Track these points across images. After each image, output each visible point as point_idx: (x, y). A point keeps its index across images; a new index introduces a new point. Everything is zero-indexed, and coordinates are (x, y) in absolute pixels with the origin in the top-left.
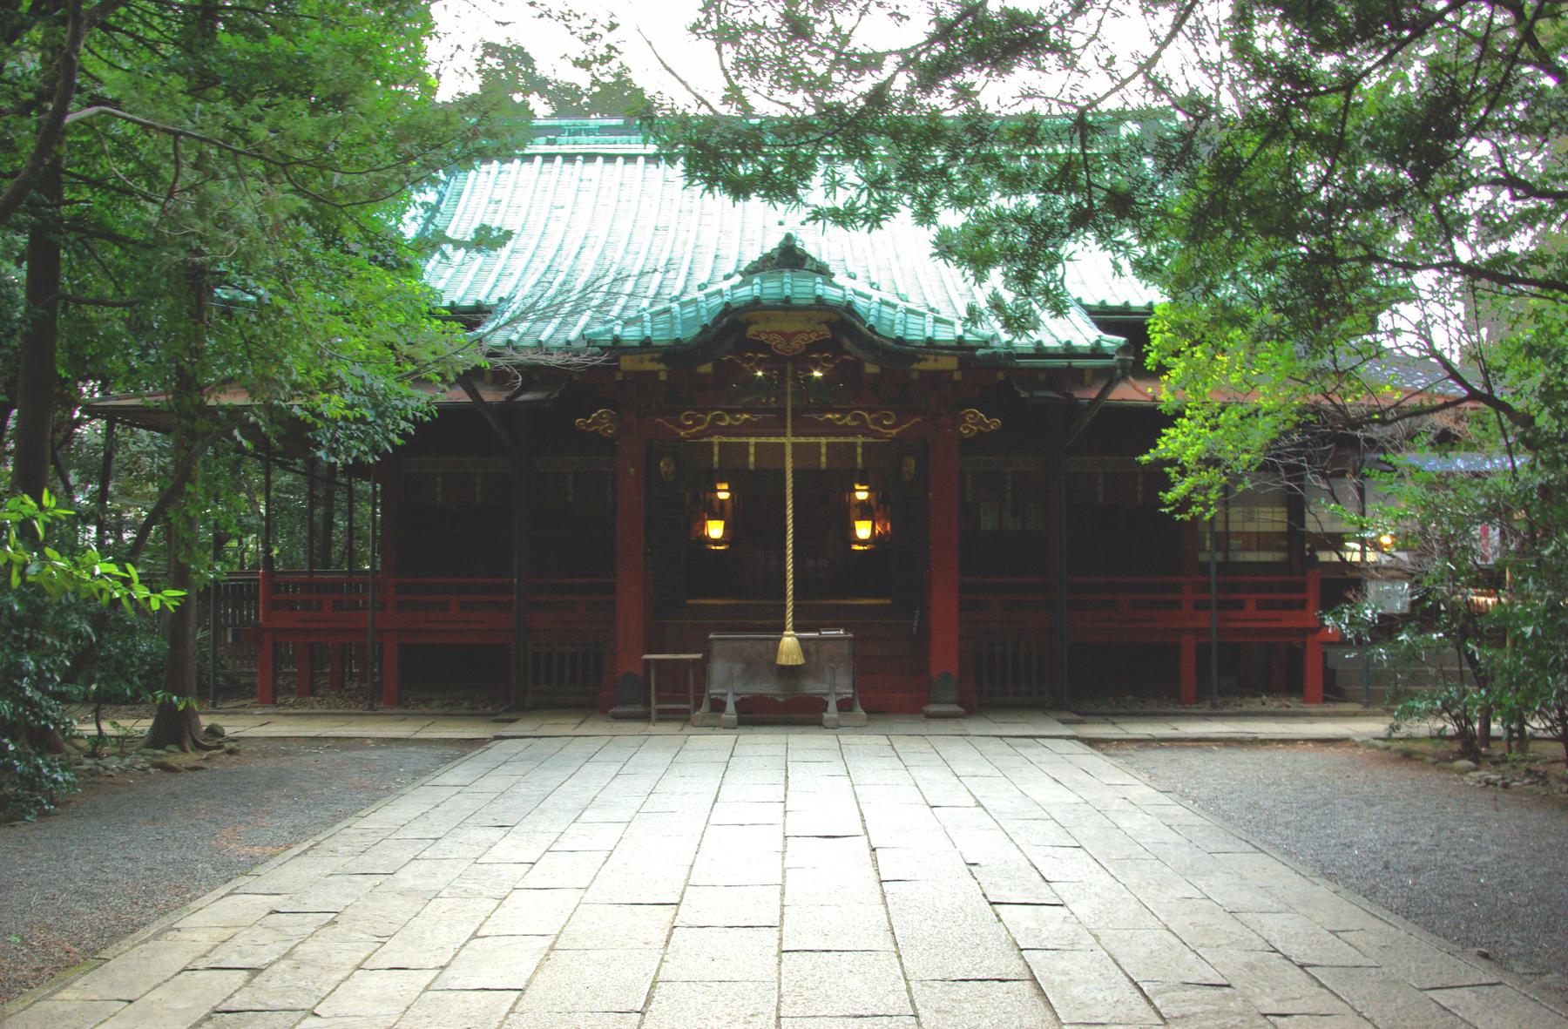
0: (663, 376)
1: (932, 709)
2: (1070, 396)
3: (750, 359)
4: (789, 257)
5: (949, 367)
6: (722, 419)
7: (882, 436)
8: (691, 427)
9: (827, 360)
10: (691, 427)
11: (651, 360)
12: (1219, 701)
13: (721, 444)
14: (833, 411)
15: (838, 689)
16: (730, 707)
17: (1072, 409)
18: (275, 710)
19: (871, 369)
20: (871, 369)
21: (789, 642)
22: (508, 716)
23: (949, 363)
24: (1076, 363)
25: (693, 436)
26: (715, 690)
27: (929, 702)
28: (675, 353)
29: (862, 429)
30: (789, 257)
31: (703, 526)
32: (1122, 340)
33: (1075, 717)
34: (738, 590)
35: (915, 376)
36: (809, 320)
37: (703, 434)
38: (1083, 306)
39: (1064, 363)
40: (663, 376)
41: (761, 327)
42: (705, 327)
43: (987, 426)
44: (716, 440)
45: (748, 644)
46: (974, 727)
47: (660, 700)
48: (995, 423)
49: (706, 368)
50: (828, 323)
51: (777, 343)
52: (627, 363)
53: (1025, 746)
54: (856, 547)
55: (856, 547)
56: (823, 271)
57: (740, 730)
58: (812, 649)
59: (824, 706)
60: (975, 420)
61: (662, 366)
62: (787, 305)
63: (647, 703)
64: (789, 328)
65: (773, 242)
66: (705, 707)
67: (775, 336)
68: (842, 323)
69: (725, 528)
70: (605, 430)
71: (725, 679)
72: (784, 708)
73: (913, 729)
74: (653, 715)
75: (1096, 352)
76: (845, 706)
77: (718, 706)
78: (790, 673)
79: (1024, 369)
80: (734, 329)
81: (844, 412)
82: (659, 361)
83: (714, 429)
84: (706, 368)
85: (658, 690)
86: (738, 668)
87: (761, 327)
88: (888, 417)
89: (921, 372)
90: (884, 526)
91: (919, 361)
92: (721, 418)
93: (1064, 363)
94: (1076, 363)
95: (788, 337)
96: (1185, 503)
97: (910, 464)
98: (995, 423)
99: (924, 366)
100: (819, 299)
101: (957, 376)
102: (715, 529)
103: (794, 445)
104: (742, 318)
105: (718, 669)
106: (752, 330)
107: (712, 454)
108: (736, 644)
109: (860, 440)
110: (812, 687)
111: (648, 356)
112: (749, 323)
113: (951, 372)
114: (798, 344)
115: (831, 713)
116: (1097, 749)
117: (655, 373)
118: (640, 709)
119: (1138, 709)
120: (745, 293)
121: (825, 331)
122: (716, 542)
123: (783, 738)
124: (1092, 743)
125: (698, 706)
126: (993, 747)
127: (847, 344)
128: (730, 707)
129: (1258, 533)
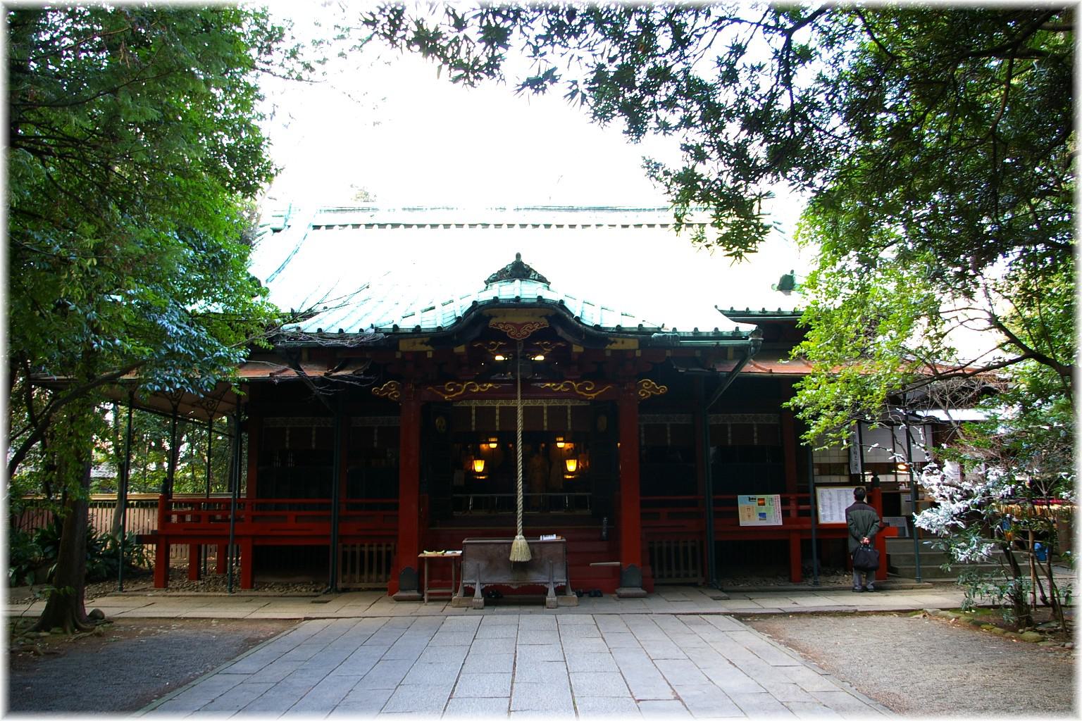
0: (430, 355)
1: (624, 591)
2: (713, 370)
3: (493, 346)
4: (519, 271)
5: (632, 348)
6: (475, 388)
7: (585, 399)
8: (452, 393)
9: (546, 346)
10: (452, 393)
11: (422, 343)
12: (822, 578)
13: (477, 408)
14: (551, 382)
15: (556, 580)
16: (478, 593)
17: (715, 379)
18: (164, 593)
19: (577, 349)
20: (577, 349)
21: (520, 541)
22: (325, 599)
23: (632, 344)
24: (723, 343)
25: (454, 400)
26: (466, 581)
27: (620, 585)
28: (438, 337)
29: (572, 394)
30: (519, 271)
31: (472, 464)
32: (753, 327)
33: (724, 595)
34: (488, 510)
35: (608, 354)
36: (533, 315)
37: (460, 398)
38: (722, 312)
39: (714, 343)
40: (430, 355)
41: (500, 320)
42: (459, 318)
43: (658, 391)
44: (474, 404)
45: (491, 547)
46: (658, 605)
47: (430, 587)
48: (663, 389)
49: (461, 349)
50: (546, 317)
51: (511, 332)
52: (404, 346)
53: (697, 624)
54: (568, 477)
55: (568, 477)
56: (542, 279)
57: (487, 610)
58: (536, 551)
59: (545, 592)
60: (648, 388)
61: (429, 347)
62: (517, 304)
63: (421, 590)
64: (519, 320)
65: (507, 260)
66: (460, 593)
67: (510, 326)
68: (554, 317)
69: (485, 465)
70: (392, 395)
71: (474, 576)
72: (515, 593)
73: (610, 609)
74: (426, 597)
75: (736, 335)
76: (560, 591)
77: (469, 592)
78: (520, 567)
79: (684, 345)
80: (481, 322)
81: (559, 381)
82: (427, 344)
83: (469, 396)
84: (461, 349)
85: (430, 578)
86: (483, 565)
87: (500, 320)
88: (589, 386)
89: (613, 351)
90: (584, 463)
91: (611, 343)
92: (473, 386)
93: (714, 343)
94: (723, 343)
95: (519, 327)
96: (821, 439)
97: (602, 422)
98: (663, 389)
99: (614, 347)
100: (540, 298)
101: (638, 353)
102: (479, 466)
103: (525, 408)
104: (486, 313)
105: (469, 567)
106: (493, 322)
107: (471, 414)
108: (482, 547)
109: (569, 403)
110: (536, 578)
111: (419, 340)
112: (491, 317)
113: (634, 351)
114: (526, 332)
115: (551, 597)
116: (746, 622)
117: (425, 353)
118: (415, 594)
119: (762, 587)
120: (487, 296)
121: (544, 322)
122: (480, 474)
123: (513, 619)
124: (741, 617)
125: (456, 591)
126: (671, 624)
127: (560, 332)
128: (478, 593)
129: (829, 464)
